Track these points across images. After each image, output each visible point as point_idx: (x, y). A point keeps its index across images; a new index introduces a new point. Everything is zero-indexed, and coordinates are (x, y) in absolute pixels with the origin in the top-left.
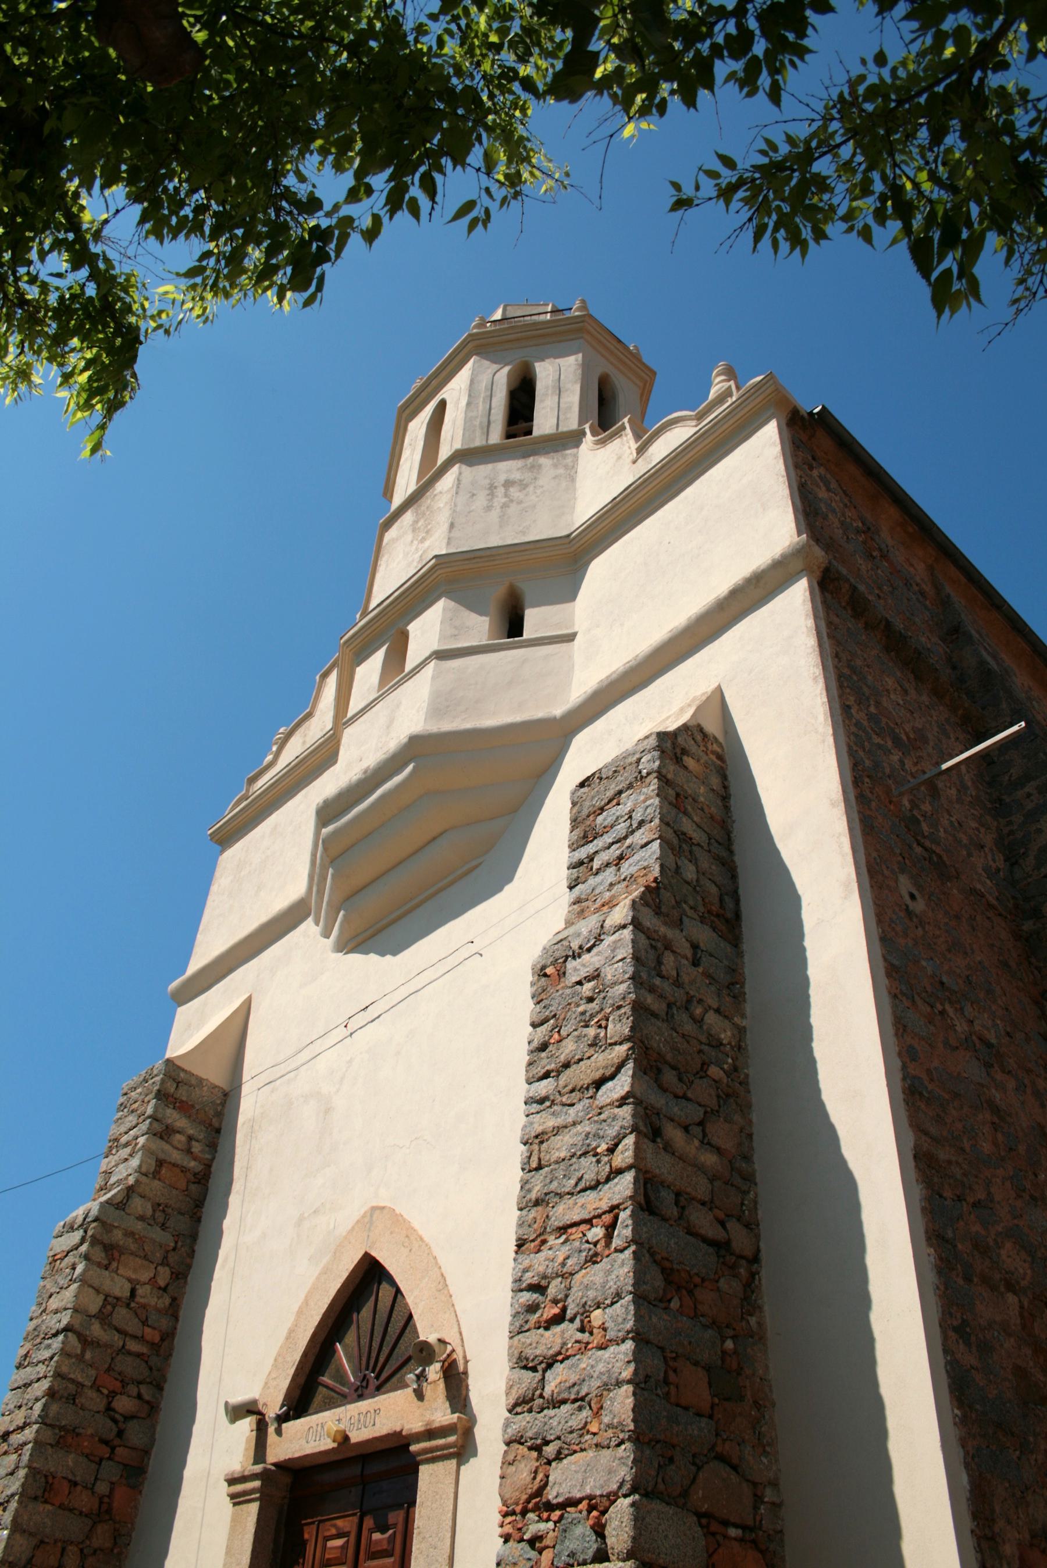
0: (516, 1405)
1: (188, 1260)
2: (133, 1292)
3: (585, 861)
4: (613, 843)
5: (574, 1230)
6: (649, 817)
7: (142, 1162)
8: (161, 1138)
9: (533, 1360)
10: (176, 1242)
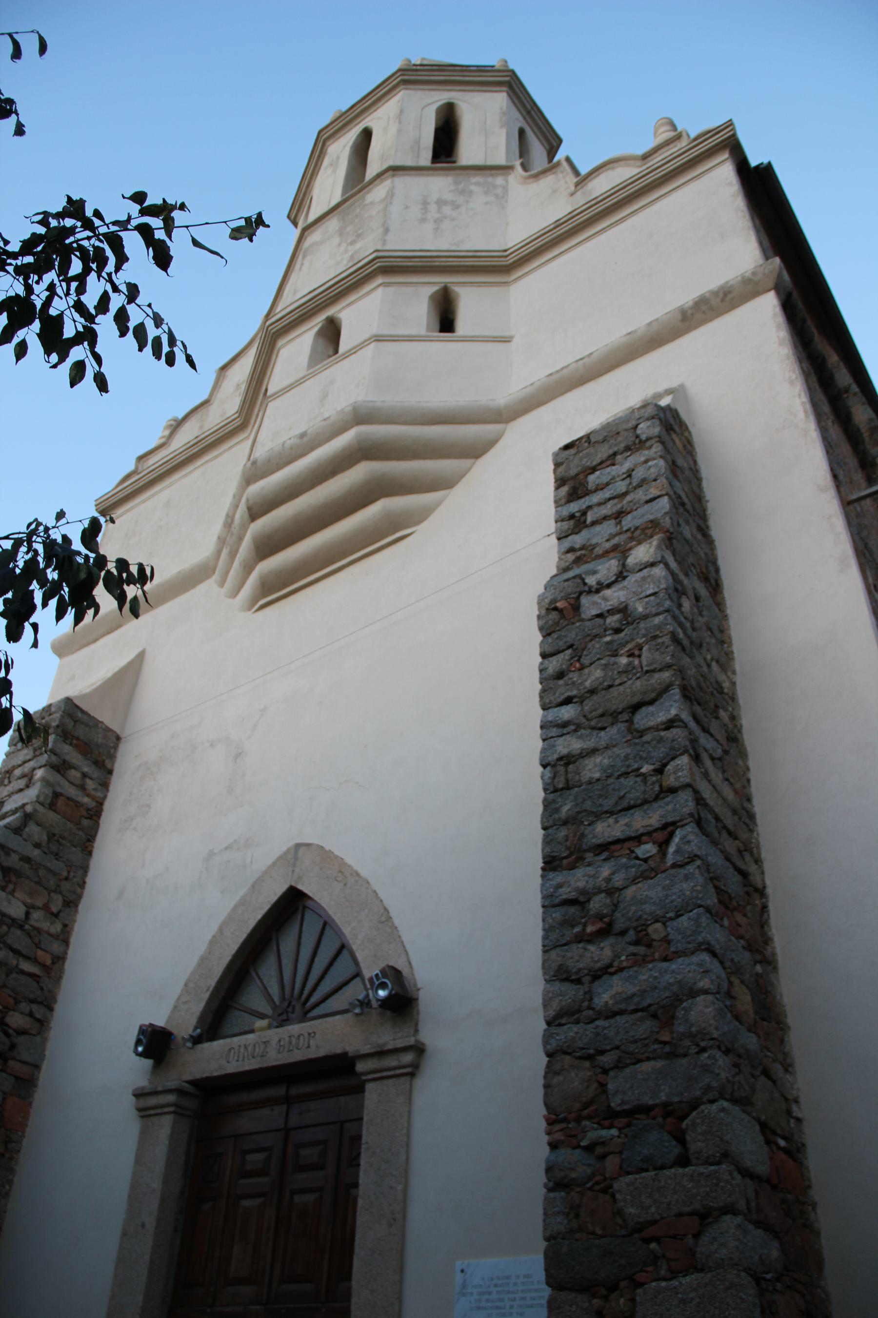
0: (558, 1016)
1: (79, 890)
2: (27, 914)
3: (577, 515)
4: (610, 499)
5: (618, 846)
6: (653, 476)
7: (40, 791)
8: (58, 771)
9: (576, 973)
10: (69, 872)
